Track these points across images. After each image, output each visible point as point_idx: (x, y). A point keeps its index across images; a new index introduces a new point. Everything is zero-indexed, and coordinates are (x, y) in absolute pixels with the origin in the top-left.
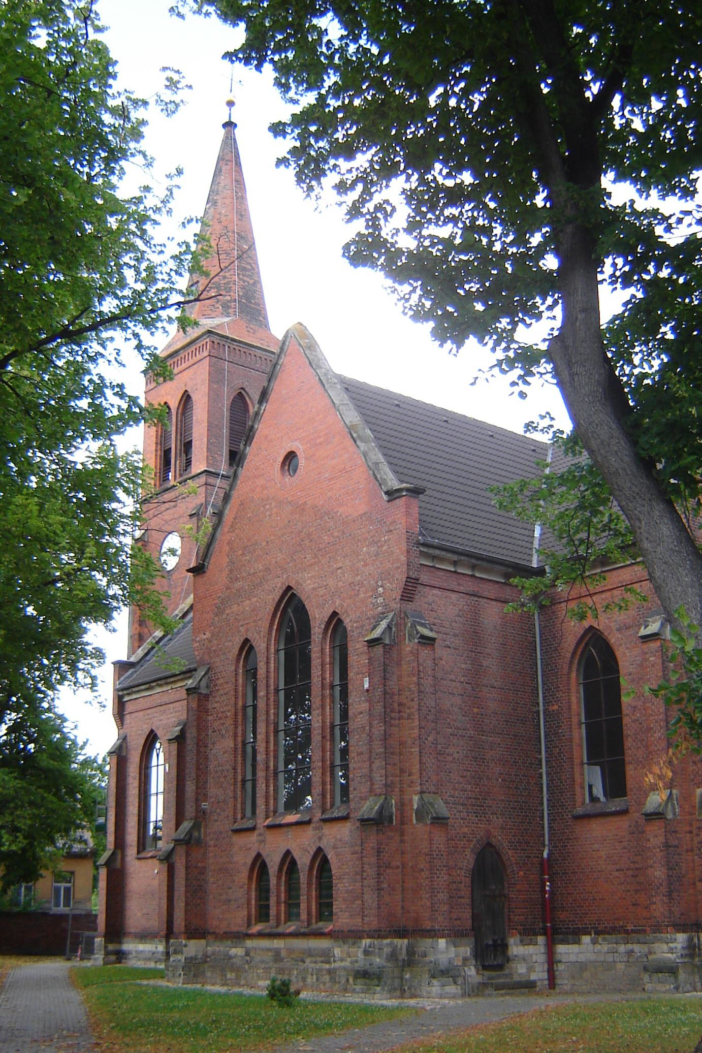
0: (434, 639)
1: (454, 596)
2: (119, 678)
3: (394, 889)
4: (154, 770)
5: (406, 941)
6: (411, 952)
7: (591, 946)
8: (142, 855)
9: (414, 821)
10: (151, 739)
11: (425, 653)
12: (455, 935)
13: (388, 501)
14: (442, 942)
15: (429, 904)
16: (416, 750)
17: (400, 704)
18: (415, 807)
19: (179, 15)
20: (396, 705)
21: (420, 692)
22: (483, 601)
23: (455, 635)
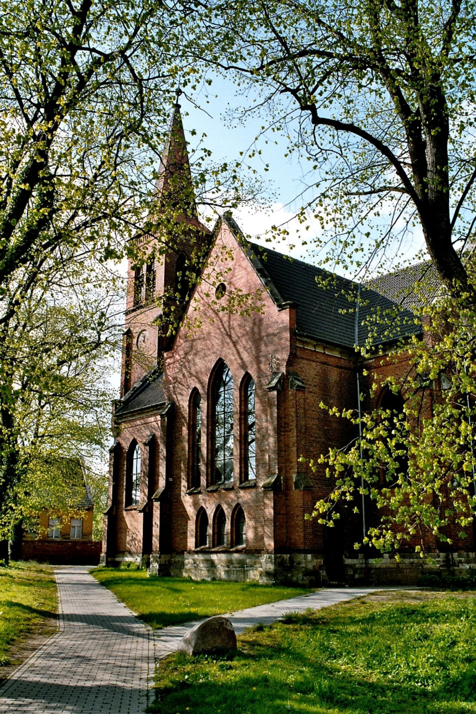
0: (304, 388)
1: (314, 364)
2: (125, 393)
3: (282, 526)
4: (135, 461)
5: (289, 555)
6: (291, 560)
7: (389, 560)
8: (129, 508)
9: (294, 489)
10: (134, 443)
11: (300, 394)
12: (315, 552)
13: (279, 311)
14: (309, 556)
15: (302, 535)
16: (295, 449)
17: (285, 423)
18: (294, 480)
19: (205, 150)
20: (283, 424)
21: (297, 416)
22: (329, 367)
23: (315, 386)
